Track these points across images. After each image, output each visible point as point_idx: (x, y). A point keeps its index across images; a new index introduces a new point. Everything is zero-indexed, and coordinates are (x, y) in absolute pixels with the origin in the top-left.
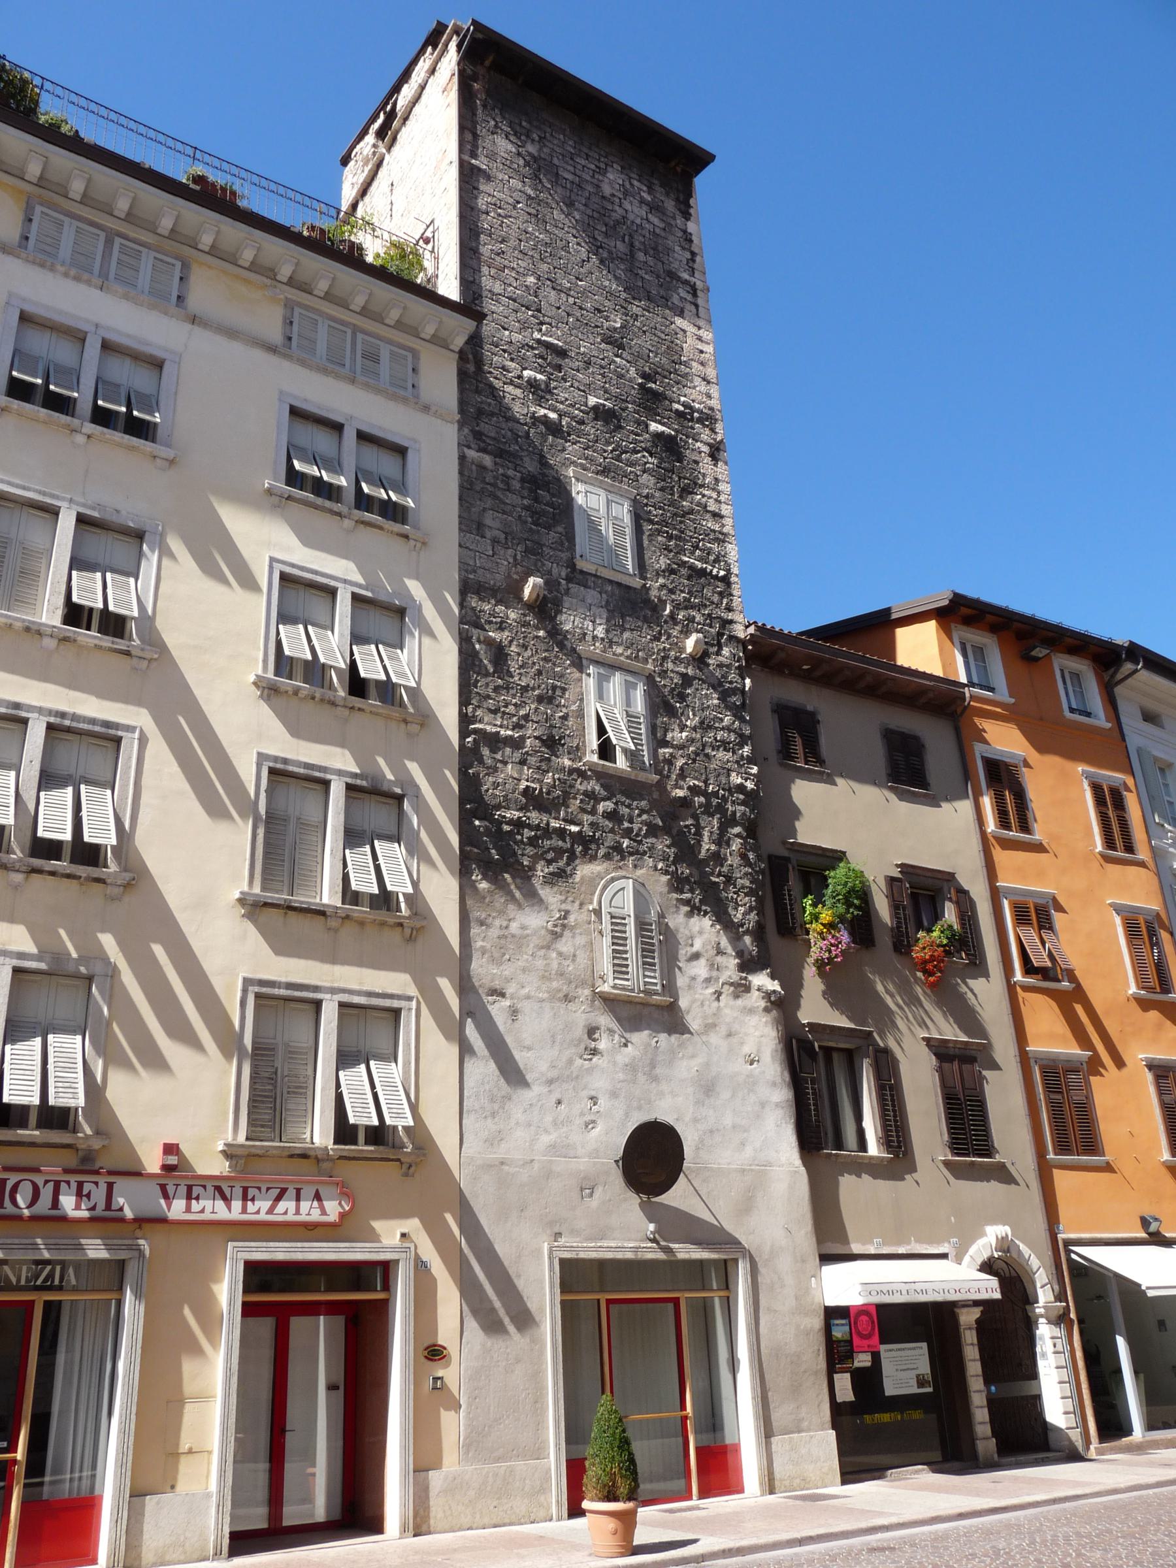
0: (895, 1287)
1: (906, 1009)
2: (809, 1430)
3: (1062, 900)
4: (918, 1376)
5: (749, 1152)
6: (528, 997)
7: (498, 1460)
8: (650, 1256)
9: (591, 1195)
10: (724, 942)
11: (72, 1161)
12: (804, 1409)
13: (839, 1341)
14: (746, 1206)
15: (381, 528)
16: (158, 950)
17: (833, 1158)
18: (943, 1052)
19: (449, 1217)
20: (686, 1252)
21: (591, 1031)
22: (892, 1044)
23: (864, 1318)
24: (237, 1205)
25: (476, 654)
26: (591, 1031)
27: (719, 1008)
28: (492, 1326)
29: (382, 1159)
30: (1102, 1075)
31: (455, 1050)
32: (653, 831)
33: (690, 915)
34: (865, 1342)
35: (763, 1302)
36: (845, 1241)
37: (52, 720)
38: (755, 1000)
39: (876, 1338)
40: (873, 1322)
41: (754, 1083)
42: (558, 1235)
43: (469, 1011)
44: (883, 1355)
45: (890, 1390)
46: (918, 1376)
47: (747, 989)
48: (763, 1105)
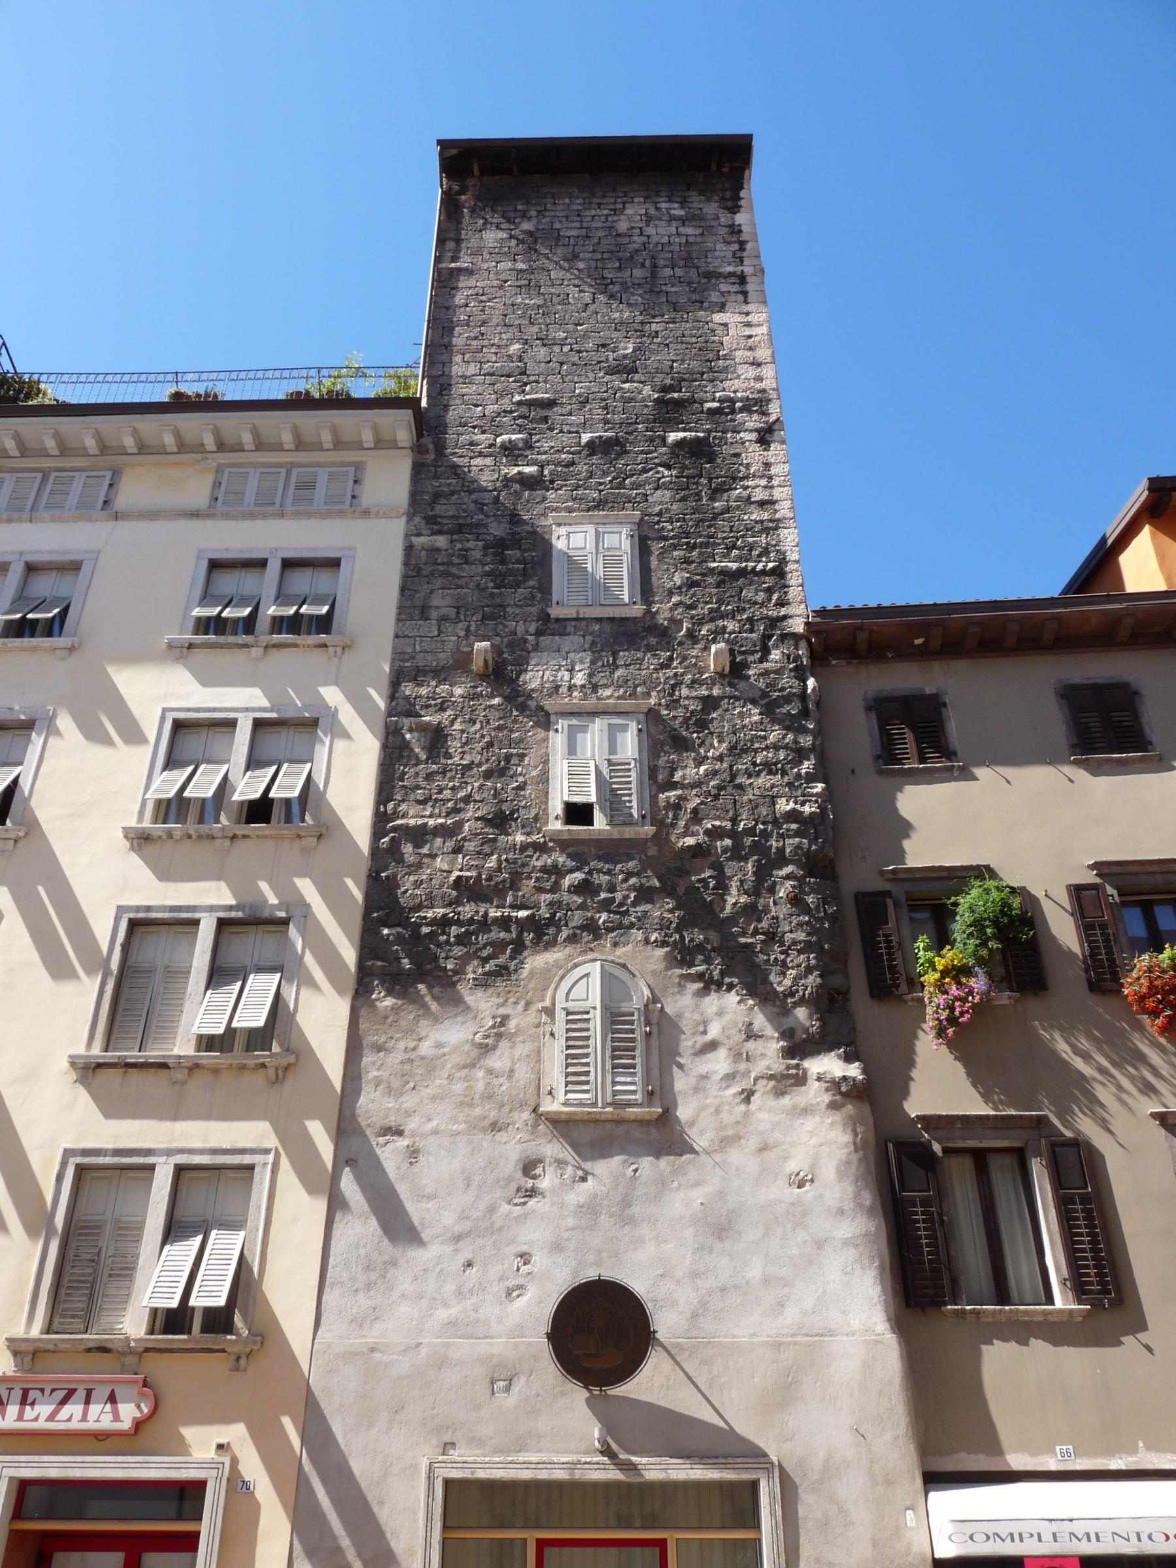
0: (1025, 1528)
6: (435, 1132)
9: (508, 1389)
15: (295, 646)
17: (971, 1318)
20: (658, 1469)
21: (529, 1167)
26: (529, 1167)
27: (746, 1114)
32: (645, 895)
33: (706, 991)
36: (996, 1450)
37: (222, 915)
38: (814, 1093)
41: (804, 1214)
43: (343, 1159)
47: (801, 1080)
48: (820, 1244)
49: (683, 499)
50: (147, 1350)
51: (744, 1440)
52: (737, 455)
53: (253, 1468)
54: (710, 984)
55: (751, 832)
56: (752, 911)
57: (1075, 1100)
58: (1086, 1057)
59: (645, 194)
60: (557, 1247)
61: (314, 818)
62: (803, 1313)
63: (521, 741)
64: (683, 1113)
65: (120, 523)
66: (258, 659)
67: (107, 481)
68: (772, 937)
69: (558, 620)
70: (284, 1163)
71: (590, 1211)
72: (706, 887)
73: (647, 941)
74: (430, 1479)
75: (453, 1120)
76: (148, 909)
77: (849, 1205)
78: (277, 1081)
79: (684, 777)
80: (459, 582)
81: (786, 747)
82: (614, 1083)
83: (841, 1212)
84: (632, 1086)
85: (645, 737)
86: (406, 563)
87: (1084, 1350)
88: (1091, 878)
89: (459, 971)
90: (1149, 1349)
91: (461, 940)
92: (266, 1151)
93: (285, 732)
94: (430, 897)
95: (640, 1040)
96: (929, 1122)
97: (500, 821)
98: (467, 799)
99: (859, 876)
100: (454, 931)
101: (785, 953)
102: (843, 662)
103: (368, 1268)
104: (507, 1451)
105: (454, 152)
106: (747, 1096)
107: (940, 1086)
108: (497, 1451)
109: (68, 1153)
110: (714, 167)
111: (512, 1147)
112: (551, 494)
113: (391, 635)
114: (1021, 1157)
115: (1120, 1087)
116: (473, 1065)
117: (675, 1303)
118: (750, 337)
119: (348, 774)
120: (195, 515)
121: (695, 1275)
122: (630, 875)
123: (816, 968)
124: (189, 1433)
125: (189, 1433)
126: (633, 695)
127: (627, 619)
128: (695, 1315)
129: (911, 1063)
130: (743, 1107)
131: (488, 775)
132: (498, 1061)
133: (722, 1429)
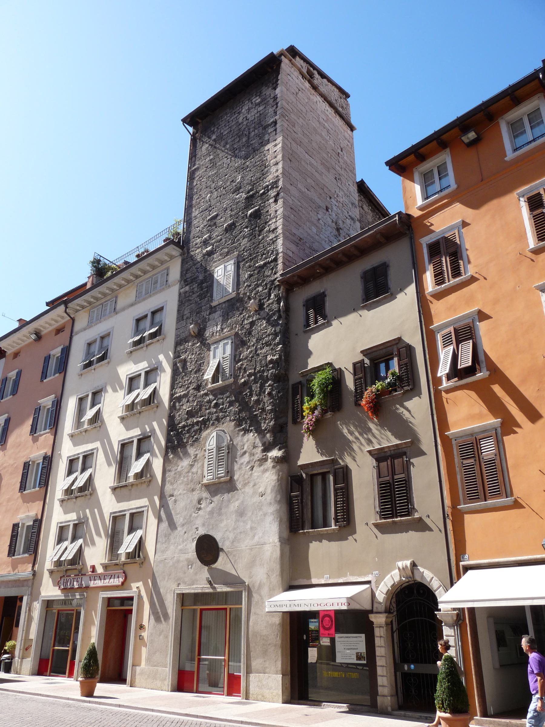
0: (283, 603)
1: (360, 438)
2: (269, 673)
3: (486, 311)
4: (357, 653)
5: (256, 538)
6: (180, 494)
7: (155, 666)
8: (207, 591)
9: (191, 568)
10: (258, 441)
11: (76, 572)
12: (267, 663)
13: (313, 631)
14: (252, 564)
15: (153, 343)
16: (96, 510)
17: (307, 534)
18: (380, 456)
19: (149, 580)
20: (221, 588)
21: (199, 502)
22: (348, 460)
23: (327, 619)
24: (102, 581)
25: (178, 368)
26: (199, 502)
27: (251, 474)
28: (158, 619)
29: (131, 563)
30: (515, 432)
31: (156, 521)
32: (231, 404)
33: (244, 434)
34: (327, 632)
35: (253, 610)
36: (309, 577)
37: (138, 438)
38: (269, 464)
39: (333, 631)
40: (332, 621)
41: (262, 506)
42: (179, 584)
43: (162, 506)
44: (337, 639)
45: (339, 659)
46: (357, 653)
47: (266, 460)
48: (265, 515)
49: (251, 240)
50: (124, 564)
51: (242, 579)
52: (268, 211)
53: (143, 593)
54: (246, 431)
55: (259, 371)
56: (258, 402)
57: (346, 450)
58: (351, 433)
59: (247, 99)
60: (204, 525)
61: (157, 401)
62: (259, 538)
63: (204, 357)
64: (236, 478)
65: (118, 315)
66: (146, 351)
67: (114, 301)
68: (263, 409)
69: (214, 307)
70: (150, 509)
71: (211, 513)
72: (246, 396)
73: (230, 420)
74: (174, 593)
75: (184, 490)
76: (124, 440)
77: (273, 501)
78: (148, 486)
79: (243, 356)
80: (191, 302)
81: (272, 334)
82: (218, 471)
83: (271, 503)
84: (222, 472)
85: (233, 344)
86: (179, 301)
87: (337, 542)
88: (360, 357)
89: (187, 442)
90: (356, 540)
91: (188, 431)
92: (146, 506)
93: (151, 374)
94: (181, 419)
95: (228, 454)
96: (303, 467)
97: (198, 388)
98: (190, 383)
99: (294, 378)
100: (186, 429)
101: (266, 415)
102: (297, 289)
103: (165, 536)
104: (190, 585)
105: (189, 120)
106: (252, 468)
107: (309, 453)
108: (188, 585)
109: (111, 513)
110: (270, 70)
111: (196, 496)
112: (215, 256)
113: (174, 329)
114: (324, 476)
115: (361, 444)
116: (189, 472)
117: (228, 538)
118: (275, 151)
119: (164, 384)
120: (132, 305)
121: (234, 529)
122: (227, 397)
123: (273, 418)
124: (132, 585)
125: (132, 585)
126: (232, 329)
127: (232, 299)
128: (233, 542)
129: (301, 446)
130: (250, 472)
131: (196, 373)
132: (194, 470)
133: (235, 575)
